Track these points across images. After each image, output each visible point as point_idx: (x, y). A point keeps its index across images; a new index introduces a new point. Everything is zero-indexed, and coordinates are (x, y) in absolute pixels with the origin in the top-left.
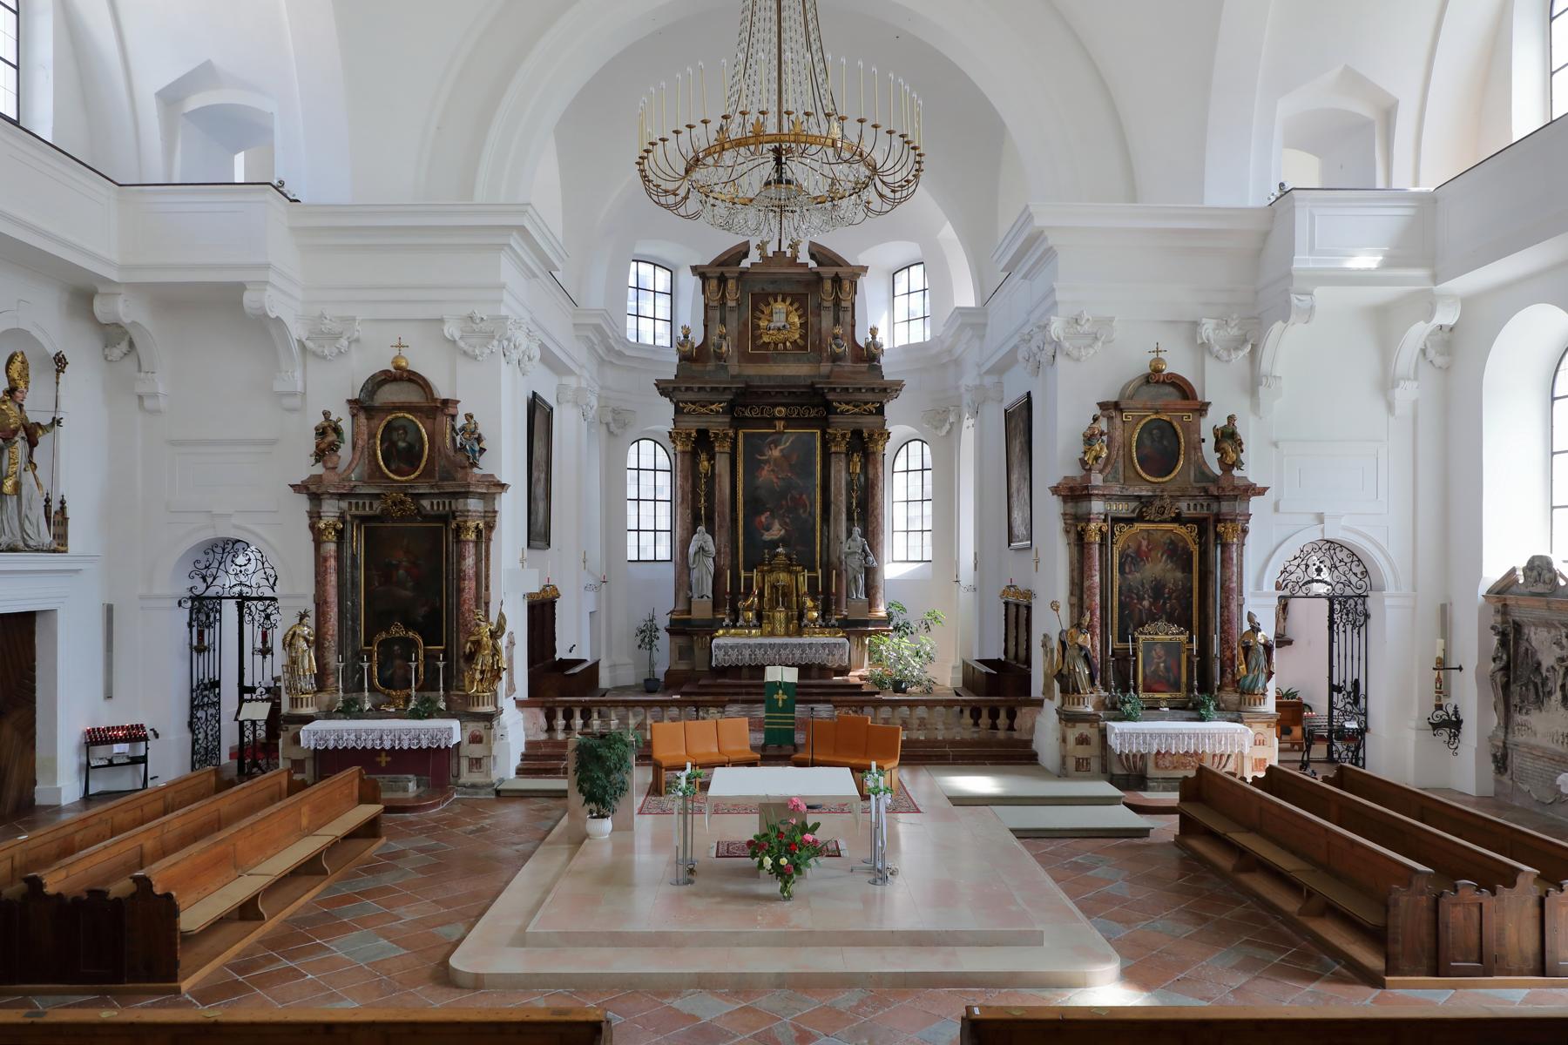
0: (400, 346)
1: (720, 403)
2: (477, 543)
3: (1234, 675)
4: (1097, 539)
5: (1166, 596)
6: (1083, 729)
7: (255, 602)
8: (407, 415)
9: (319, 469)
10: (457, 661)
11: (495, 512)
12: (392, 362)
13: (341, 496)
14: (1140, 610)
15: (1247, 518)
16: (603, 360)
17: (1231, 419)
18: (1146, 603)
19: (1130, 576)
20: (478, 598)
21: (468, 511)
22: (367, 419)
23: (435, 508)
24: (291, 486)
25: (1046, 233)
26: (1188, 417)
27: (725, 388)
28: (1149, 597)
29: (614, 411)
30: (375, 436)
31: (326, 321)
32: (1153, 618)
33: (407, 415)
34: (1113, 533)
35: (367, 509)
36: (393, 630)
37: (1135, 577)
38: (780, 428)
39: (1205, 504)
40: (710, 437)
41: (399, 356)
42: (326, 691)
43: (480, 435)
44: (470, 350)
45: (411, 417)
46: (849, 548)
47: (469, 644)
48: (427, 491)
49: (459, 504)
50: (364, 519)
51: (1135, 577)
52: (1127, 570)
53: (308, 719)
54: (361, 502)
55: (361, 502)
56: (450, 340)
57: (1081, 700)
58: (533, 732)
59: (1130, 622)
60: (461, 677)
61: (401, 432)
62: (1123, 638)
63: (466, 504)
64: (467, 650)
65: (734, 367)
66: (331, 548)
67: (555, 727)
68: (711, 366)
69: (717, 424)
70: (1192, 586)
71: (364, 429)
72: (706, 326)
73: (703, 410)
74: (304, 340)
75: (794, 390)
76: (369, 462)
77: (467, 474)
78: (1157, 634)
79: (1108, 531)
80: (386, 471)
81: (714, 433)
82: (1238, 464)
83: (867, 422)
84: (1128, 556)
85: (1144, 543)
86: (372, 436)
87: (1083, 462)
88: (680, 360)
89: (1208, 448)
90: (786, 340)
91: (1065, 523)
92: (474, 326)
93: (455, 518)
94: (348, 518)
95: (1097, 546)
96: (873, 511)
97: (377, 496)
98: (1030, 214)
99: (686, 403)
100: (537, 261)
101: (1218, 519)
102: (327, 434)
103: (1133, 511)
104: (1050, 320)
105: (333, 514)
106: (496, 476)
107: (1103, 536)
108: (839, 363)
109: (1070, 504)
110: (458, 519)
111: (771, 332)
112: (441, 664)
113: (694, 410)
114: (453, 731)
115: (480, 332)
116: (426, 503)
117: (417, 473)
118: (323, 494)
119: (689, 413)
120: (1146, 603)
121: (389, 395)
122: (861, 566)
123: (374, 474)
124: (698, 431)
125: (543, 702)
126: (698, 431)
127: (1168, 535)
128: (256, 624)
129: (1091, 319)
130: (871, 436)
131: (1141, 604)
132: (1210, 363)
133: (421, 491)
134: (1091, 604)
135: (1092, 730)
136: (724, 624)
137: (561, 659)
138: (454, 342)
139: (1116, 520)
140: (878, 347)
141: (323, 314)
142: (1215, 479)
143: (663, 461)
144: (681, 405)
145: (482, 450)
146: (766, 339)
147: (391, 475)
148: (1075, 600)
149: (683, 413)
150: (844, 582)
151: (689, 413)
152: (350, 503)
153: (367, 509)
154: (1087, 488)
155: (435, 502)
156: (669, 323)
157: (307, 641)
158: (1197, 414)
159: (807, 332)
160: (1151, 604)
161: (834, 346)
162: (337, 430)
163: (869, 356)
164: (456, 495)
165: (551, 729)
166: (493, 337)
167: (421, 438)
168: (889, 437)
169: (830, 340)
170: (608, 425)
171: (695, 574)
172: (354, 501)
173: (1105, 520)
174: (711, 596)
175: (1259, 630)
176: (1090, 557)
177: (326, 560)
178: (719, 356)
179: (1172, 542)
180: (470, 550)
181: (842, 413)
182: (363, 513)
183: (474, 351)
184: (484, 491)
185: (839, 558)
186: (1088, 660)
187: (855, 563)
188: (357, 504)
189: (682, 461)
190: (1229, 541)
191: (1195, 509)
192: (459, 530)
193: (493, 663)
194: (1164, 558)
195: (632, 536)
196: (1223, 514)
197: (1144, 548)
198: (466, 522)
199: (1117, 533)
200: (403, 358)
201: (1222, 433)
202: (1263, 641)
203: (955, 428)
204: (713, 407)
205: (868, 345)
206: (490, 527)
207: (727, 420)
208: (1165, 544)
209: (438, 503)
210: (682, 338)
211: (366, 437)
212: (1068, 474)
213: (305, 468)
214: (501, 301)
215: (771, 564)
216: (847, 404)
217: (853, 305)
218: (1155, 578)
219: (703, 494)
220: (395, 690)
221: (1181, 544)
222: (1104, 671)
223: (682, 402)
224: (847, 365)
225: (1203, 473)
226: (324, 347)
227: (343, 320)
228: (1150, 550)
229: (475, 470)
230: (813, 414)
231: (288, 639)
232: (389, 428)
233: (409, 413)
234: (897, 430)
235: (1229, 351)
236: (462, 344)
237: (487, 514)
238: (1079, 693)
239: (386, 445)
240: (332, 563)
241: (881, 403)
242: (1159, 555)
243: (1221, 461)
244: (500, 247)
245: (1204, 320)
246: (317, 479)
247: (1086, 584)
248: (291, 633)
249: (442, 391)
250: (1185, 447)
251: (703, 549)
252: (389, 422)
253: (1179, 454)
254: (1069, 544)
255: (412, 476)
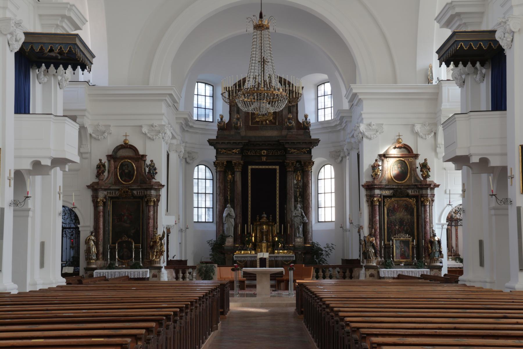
0: (126, 136)
1: (237, 149)
2: (154, 206)
3: (428, 253)
4: (377, 204)
5: (405, 224)
6: (372, 271)
7: (67, 230)
8: (129, 160)
9: (97, 180)
10: (146, 249)
11: (160, 195)
12: (124, 142)
13: (105, 190)
14: (395, 230)
15: (433, 196)
16: (184, 129)
17: (425, 160)
18: (397, 227)
19: (391, 217)
20: (154, 226)
21: (152, 195)
22: (114, 162)
23: (138, 194)
24: (87, 186)
25: (358, 94)
26: (411, 160)
27: (239, 143)
28: (398, 225)
29: (188, 153)
30: (117, 168)
31: (100, 127)
32: (399, 232)
33: (129, 160)
34: (384, 202)
35: (114, 194)
36: (123, 238)
37: (393, 218)
38: (264, 160)
39: (418, 191)
40: (232, 164)
41: (126, 140)
42: (99, 260)
43: (155, 168)
44: (151, 137)
45: (130, 161)
46: (295, 214)
47: (152, 243)
48: (136, 188)
49: (148, 192)
50: (111, 198)
51: (393, 218)
52: (390, 215)
53: (96, 269)
54: (111, 192)
55: (111, 192)
56: (143, 133)
57: (371, 261)
58: (171, 278)
59: (391, 233)
60: (148, 254)
61: (126, 166)
62: (389, 240)
63: (151, 192)
64: (151, 245)
65: (243, 132)
66: (101, 208)
67: (179, 277)
68: (233, 132)
69: (236, 159)
70: (414, 221)
71: (113, 165)
72: (230, 114)
73: (229, 152)
74: (92, 133)
75: (271, 143)
76: (115, 177)
77: (151, 182)
78: (400, 238)
79: (381, 201)
80: (121, 180)
81: (234, 163)
82: (428, 176)
83: (303, 157)
84: (390, 210)
85: (396, 205)
86: (116, 168)
87: (372, 176)
88: (219, 129)
89: (418, 170)
90: (267, 120)
91: (367, 198)
92: (153, 128)
93: (146, 197)
94: (107, 197)
95: (378, 206)
96: (306, 197)
97: (118, 190)
98: (351, 88)
99: (222, 149)
100: (171, 100)
101: (422, 196)
102: (100, 167)
103: (391, 194)
104: (360, 125)
105: (102, 196)
106: (160, 182)
107: (380, 202)
108: (290, 131)
109: (368, 191)
110: (148, 198)
111: (260, 116)
112: (141, 250)
113: (225, 153)
114: (148, 273)
115: (155, 130)
116: (135, 192)
117: (132, 181)
118: (100, 189)
119: (223, 154)
120: (397, 227)
121: (122, 153)
122: (301, 222)
123: (117, 182)
124: (227, 162)
125: (175, 267)
126: (227, 162)
127: (405, 202)
128: (68, 238)
129: (375, 124)
130: (305, 163)
131: (395, 228)
132: (420, 140)
133: (134, 188)
134: (375, 227)
135: (375, 272)
136: (238, 249)
137: (171, 260)
138: (146, 134)
139: (385, 197)
140: (308, 123)
141: (99, 124)
142: (421, 181)
143: (209, 175)
144: (219, 150)
145: (156, 173)
146: (257, 120)
147: (122, 182)
148: (370, 226)
149: (221, 154)
150: (293, 229)
151: (223, 154)
152: (108, 192)
153: (114, 194)
154: (372, 185)
155: (138, 192)
156: (212, 110)
157: (94, 242)
158: (414, 158)
159: (276, 116)
160: (399, 228)
161: (288, 123)
162: (104, 166)
163: (305, 127)
164: (147, 189)
165: (177, 278)
166: (160, 132)
167: (134, 169)
168: (313, 164)
169: (286, 120)
170: (186, 159)
171: (226, 226)
172: (109, 191)
173: (380, 197)
174: (233, 236)
175: (436, 236)
176: (375, 210)
177: (99, 212)
178: (237, 128)
179: (406, 205)
180: (152, 208)
181: (292, 153)
182: (112, 196)
183: (153, 137)
184: (157, 188)
185: (291, 219)
186: (373, 246)
187: (297, 220)
188: (110, 192)
189: (220, 175)
190: (426, 204)
191: (414, 193)
192: (148, 202)
193: (160, 249)
194: (403, 211)
195: (195, 210)
196: (423, 194)
197: (396, 207)
198: (151, 199)
199: (386, 202)
200: (127, 140)
201: (423, 165)
202: (437, 240)
203: (344, 159)
204: (234, 151)
205: (303, 122)
206: (158, 200)
207: (240, 157)
208: (404, 205)
209: (140, 192)
210: (220, 120)
211: (113, 168)
212: (368, 180)
213: (91, 179)
214: (162, 119)
215: (260, 222)
216: (294, 149)
217: (297, 105)
218: (400, 219)
219: (229, 190)
220: (124, 260)
221: (410, 206)
222: (381, 251)
223: (220, 149)
224: (294, 131)
225: (416, 180)
226: (99, 136)
227: (105, 126)
228: (398, 208)
229: (154, 180)
230: (279, 153)
231: (87, 240)
232: (122, 165)
233: (130, 160)
234: (317, 160)
235: (426, 135)
236: (149, 135)
237: (157, 196)
238: (371, 259)
239: (121, 171)
240: (101, 214)
241: (309, 148)
242: (402, 210)
243: (422, 175)
244: (162, 100)
245: (416, 124)
246: (97, 183)
247: (374, 220)
248: (88, 238)
249: (141, 153)
250: (410, 170)
251: (229, 214)
252: (122, 163)
253: (408, 173)
254: (368, 206)
255: (130, 182)
